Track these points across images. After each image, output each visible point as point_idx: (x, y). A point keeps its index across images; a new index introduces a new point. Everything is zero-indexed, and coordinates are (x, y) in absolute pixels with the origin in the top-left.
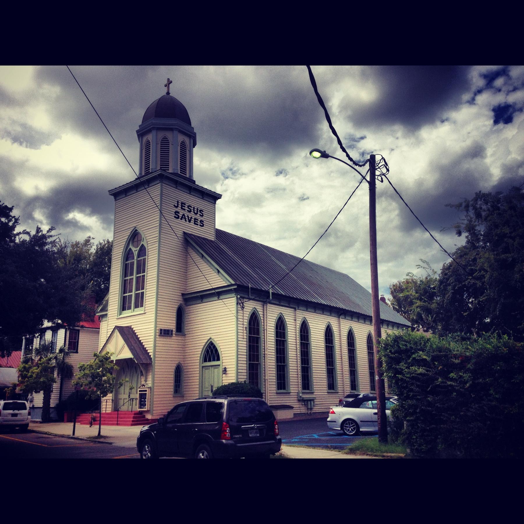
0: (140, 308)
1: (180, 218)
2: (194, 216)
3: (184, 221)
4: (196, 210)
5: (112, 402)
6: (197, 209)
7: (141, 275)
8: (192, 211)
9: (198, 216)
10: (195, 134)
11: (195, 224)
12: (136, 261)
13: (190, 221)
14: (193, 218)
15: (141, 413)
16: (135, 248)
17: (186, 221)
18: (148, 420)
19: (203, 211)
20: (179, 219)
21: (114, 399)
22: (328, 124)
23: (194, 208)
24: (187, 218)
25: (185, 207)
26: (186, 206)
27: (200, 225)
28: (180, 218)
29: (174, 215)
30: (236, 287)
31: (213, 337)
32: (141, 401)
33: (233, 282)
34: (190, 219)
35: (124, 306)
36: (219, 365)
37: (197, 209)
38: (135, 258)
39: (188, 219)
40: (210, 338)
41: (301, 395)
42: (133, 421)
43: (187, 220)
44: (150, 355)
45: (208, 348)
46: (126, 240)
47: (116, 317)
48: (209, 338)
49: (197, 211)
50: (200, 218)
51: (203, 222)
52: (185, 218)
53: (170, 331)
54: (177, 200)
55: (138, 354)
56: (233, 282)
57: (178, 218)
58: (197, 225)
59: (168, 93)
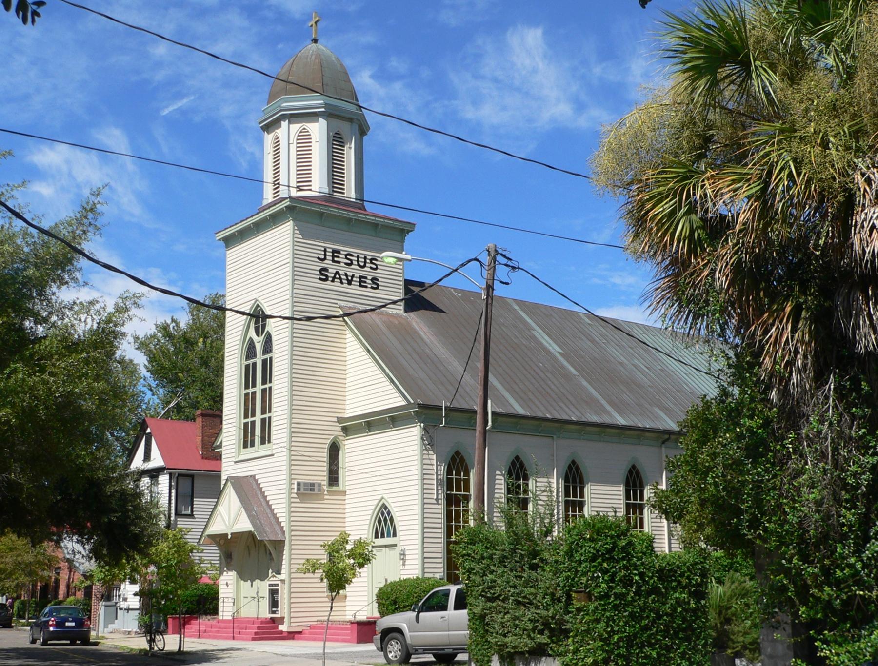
1: (330, 279)
3: (340, 284)
6: (365, 258)
9: (368, 272)
11: (360, 286)
13: (350, 283)
15: (273, 620)
17: (342, 283)
18: (281, 632)
19: (376, 260)
20: (328, 282)
23: (358, 257)
24: (344, 277)
25: (338, 257)
26: (341, 256)
27: (372, 288)
28: (330, 279)
31: (385, 496)
34: (350, 278)
35: (248, 441)
36: (395, 545)
37: (365, 258)
39: (347, 279)
40: (382, 498)
42: (256, 633)
44: (283, 527)
45: (380, 514)
47: (233, 459)
48: (380, 497)
49: (365, 262)
51: (378, 280)
52: (340, 278)
53: (316, 486)
57: (326, 280)
58: (366, 287)
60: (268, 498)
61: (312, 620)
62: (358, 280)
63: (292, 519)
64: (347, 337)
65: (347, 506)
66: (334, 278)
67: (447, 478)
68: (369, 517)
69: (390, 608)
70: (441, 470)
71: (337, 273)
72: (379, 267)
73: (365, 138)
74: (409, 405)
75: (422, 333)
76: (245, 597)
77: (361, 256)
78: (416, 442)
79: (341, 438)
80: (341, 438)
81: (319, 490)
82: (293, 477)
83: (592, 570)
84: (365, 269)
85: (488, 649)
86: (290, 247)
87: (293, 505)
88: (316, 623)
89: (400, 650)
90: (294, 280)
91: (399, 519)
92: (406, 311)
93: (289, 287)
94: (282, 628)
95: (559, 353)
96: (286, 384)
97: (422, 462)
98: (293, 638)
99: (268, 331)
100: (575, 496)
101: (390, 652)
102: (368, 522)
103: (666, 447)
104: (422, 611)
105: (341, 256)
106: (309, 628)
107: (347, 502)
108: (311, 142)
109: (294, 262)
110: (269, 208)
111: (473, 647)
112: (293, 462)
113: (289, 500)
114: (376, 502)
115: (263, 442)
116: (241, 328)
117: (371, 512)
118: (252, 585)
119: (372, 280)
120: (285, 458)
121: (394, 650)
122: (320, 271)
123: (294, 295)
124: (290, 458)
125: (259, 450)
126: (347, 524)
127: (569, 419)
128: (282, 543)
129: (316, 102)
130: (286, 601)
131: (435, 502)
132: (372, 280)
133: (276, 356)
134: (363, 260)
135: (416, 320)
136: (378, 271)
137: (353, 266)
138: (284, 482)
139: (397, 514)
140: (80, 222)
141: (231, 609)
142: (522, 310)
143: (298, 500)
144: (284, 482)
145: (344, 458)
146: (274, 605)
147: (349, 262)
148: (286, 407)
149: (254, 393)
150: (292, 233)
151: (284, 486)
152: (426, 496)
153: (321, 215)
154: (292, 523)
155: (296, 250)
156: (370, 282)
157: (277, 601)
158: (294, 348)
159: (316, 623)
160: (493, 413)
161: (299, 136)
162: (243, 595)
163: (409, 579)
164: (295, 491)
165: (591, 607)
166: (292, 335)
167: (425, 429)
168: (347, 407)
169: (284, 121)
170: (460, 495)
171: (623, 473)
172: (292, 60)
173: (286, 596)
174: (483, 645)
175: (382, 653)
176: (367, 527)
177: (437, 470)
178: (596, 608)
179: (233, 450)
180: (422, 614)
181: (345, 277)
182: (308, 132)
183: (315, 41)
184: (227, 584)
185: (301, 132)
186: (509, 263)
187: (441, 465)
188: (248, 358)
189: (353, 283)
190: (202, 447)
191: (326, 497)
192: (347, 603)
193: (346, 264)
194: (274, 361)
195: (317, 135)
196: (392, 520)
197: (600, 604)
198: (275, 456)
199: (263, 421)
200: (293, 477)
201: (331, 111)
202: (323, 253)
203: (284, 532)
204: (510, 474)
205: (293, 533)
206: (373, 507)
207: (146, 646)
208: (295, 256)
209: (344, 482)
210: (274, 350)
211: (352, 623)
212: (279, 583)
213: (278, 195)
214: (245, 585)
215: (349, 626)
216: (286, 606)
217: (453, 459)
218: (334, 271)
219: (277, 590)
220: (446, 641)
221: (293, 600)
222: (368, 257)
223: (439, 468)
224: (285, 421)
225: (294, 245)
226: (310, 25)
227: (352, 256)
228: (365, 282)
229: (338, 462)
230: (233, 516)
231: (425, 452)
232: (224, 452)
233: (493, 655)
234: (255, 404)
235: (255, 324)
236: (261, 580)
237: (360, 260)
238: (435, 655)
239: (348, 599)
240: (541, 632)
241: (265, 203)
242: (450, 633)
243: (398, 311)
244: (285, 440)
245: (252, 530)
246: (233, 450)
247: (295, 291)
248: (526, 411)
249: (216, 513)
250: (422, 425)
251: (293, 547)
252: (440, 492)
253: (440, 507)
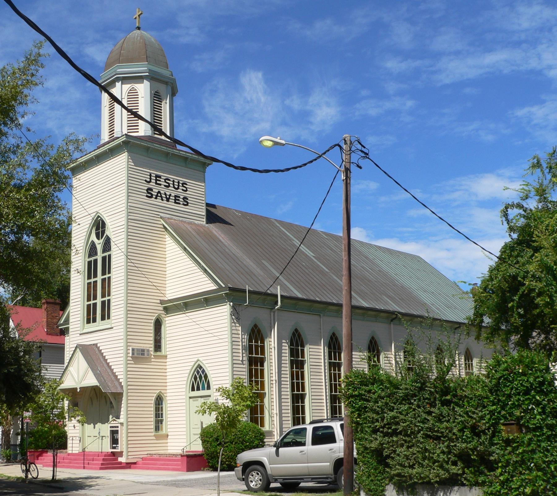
1: (154, 197)
3: (161, 201)
6: (179, 183)
8: (172, 185)
11: (175, 203)
13: (168, 200)
14: (173, 195)
15: (113, 454)
17: (162, 200)
18: (121, 463)
19: (186, 184)
20: (153, 199)
22: (280, 172)
23: (173, 181)
25: (160, 181)
26: (161, 180)
27: (184, 204)
28: (154, 197)
29: (145, 195)
31: (201, 359)
34: (168, 197)
35: (90, 318)
36: (210, 396)
37: (179, 183)
39: (166, 197)
40: (198, 360)
42: (102, 464)
44: (121, 383)
45: (196, 373)
46: (87, 230)
47: (79, 332)
48: (196, 360)
49: (179, 186)
50: (182, 195)
51: (187, 199)
52: (161, 196)
53: (146, 351)
55: (105, 381)
57: (151, 197)
58: (179, 204)
60: (108, 361)
61: (143, 454)
62: (174, 198)
63: (129, 376)
64: (167, 240)
65: (168, 367)
66: (157, 196)
67: (249, 344)
68: (187, 375)
69: (213, 444)
70: (245, 339)
71: (159, 192)
72: (188, 189)
73: (174, 98)
74: (220, 288)
75: (221, 238)
76: (88, 436)
77: (175, 181)
78: (226, 317)
79: (163, 316)
80: (163, 316)
81: (148, 355)
82: (129, 344)
83: (526, 402)
84: (179, 190)
85: (382, 480)
86: (126, 172)
87: (129, 366)
88: (146, 456)
89: (260, 480)
90: (128, 196)
91: (212, 376)
92: (207, 223)
93: (125, 201)
94: (120, 459)
95: (313, 256)
96: (123, 274)
97: (231, 332)
98: (130, 468)
99: (107, 235)
100: (335, 359)
101: (252, 482)
102: (186, 379)
103: (394, 324)
104: (281, 447)
105: (161, 180)
106: (141, 460)
107: (167, 364)
108: (138, 98)
109: (128, 183)
110: (104, 146)
111: (364, 478)
112: (129, 333)
113: (126, 362)
114: (192, 364)
115: (103, 318)
116: (85, 234)
117: (188, 371)
118: (94, 427)
119: (183, 199)
120: (122, 330)
121: (255, 480)
122: (147, 190)
123: (129, 207)
124: (126, 330)
125: (100, 324)
126: (168, 381)
127: (331, 302)
128: (121, 395)
129: (141, 68)
130: (124, 439)
131: (241, 363)
132: (183, 199)
133: (114, 253)
134: (177, 184)
135: (214, 228)
136: (187, 192)
137: (170, 188)
138: (122, 348)
139: (211, 372)
140: (24, 71)
141: (78, 445)
142: (282, 227)
143: (133, 363)
144: (122, 348)
145: (165, 331)
146: (115, 441)
147: (168, 185)
148: (123, 291)
149: (95, 282)
150: (127, 161)
151: (122, 352)
152: (234, 358)
153: (147, 149)
154: (129, 380)
155: (130, 174)
156: (182, 200)
157: (118, 439)
158: (129, 247)
159: (146, 456)
160: (282, 296)
161: (129, 93)
162: (86, 435)
164: (130, 355)
165: (526, 440)
166: (127, 237)
167: (233, 307)
168: (167, 292)
169: (118, 82)
170: (258, 357)
171: (366, 342)
172: (123, 40)
173: (124, 435)
174: (376, 476)
175: (244, 482)
176: (185, 382)
177: (242, 338)
178: (530, 440)
179: (79, 325)
180: (281, 449)
181: (164, 196)
182: (136, 90)
183: (139, 28)
184: (74, 426)
185: (130, 90)
186: (363, 149)
187: (245, 335)
188: (90, 256)
189: (170, 200)
190: (47, 326)
191: (153, 360)
192: (169, 441)
193: (165, 186)
194: (112, 257)
195: (143, 92)
196: (206, 376)
197: (534, 436)
198: (114, 328)
199: (103, 303)
200: (129, 344)
201: (153, 76)
202: (149, 177)
203: (122, 387)
204: (292, 344)
205: (129, 387)
206: (190, 368)
207: (23, 475)
208: (130, 178)
209: (165, 348)
210: (112, 249)
211: (182, 456)
212: (119, 425)
213: (113, 136)
214: (89, 428)
215: (179, 457)
216: (124, 443)
217: (253, 330)
218: (157, 191)
219: (118, 431)
220: (306, 472)
221: (129, 438)
222: (180, 182)
223: (243, 337)
224: (123, 302)
225: (128, 170)
226: (134, 17)
227: (169, 180)
228: (179, 200)
229: (161, 333)
230: (81, 374)
231: (233, 324)
232: (71, 327)
233: (388, 484)
234: (96, 290)
235: (96, 231)
236: (102, 424)
237: (175, 183)
238: (281, 484)
239: (169, 437)
240: (455, 463)
241: (102, 142)
242: (309, 464)
243: (202, 223)
244: (122, 316)
245: (98, 384)
246: (79, 325)
247: (129, 204)
248: (302, 295)
249: (67, 372)
250: (231, 304)
251: (129, 398)
252: (244, 355)
253: (244, 366)
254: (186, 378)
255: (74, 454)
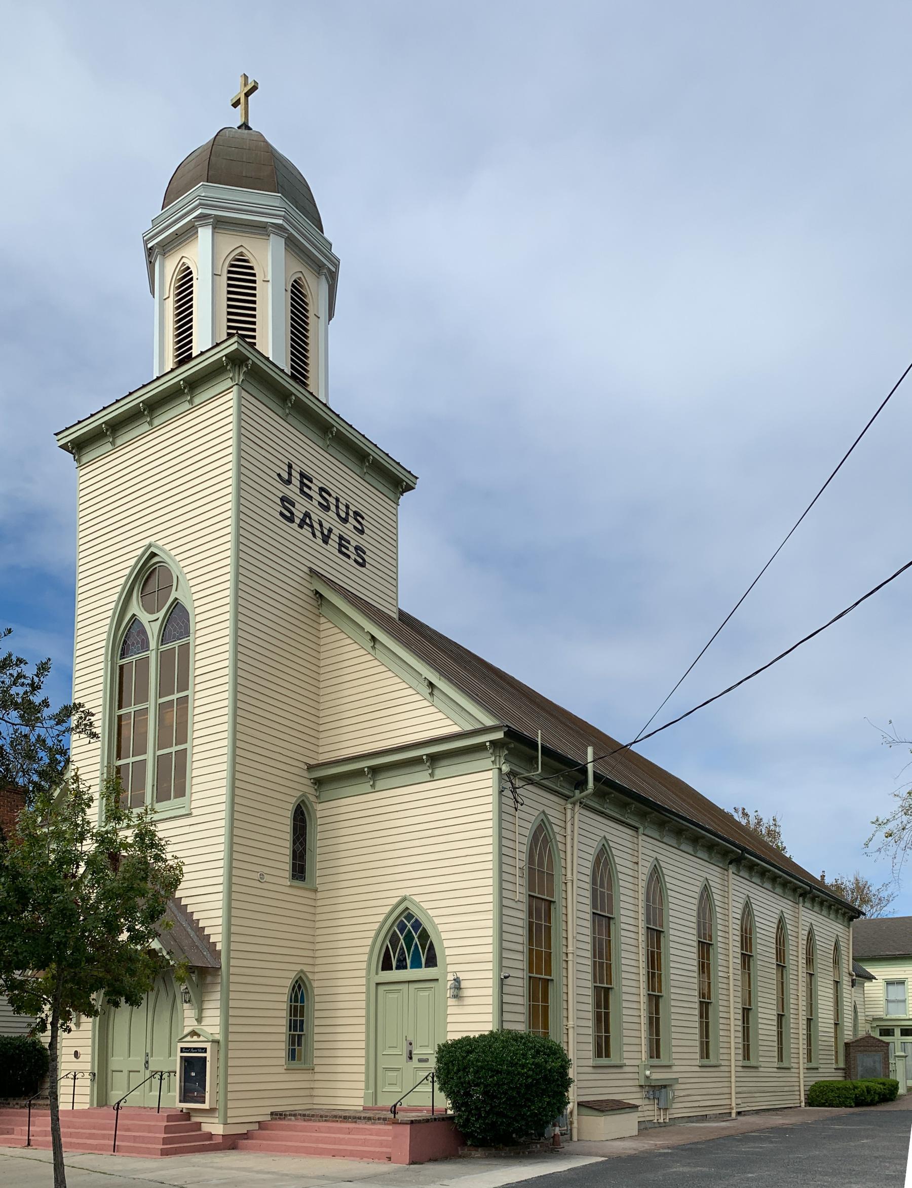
0: (174, 802)
2: (339, 529)
3: (341, 499)
4: (344, 509)
5: (92, 1080)
7: (174, 697)
8: (333, 508)
9: (348, 530)
10: (336, 263)
12: (154, 653)
16: (151, 612)
18: (210, 1136)
20: (295, 526)
21: (96, 1072)
23: (337, 500)
24: (316, 526)
28: (297, 521)
30: (499, 735)
32: (186, 1078)
33: (489, 721)
34: (326, 532)
37: (347, 507)
38: (153, 644)
39: (322, 533)
41: (648, 1073)
42: (165, 1141)
43: (318, 534)
44: (214, 944)
46: (127, 571)
50: (355, 539)
52: (312, 526)
54: (286, 461)
56: (489, 721)
59: (245, 126)
163: (468, 1038)
254: (371, 940)
255: (78, 1111)
